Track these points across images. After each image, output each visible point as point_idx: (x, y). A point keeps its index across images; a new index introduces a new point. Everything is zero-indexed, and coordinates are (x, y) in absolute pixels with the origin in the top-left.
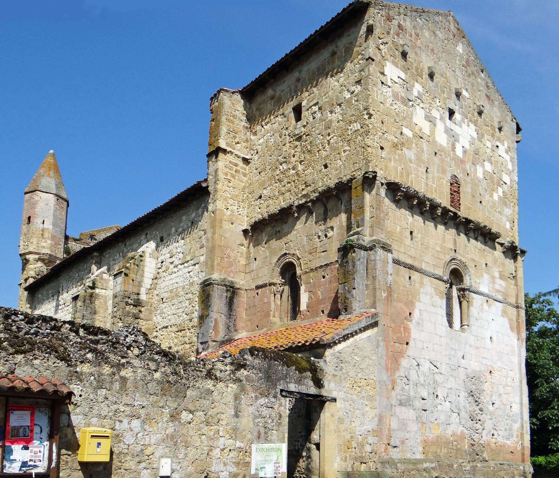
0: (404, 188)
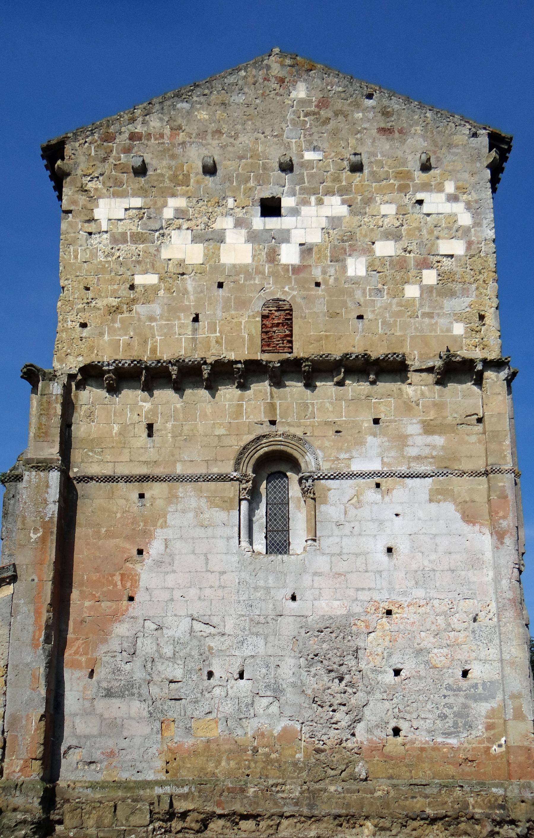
0: (108, 365)
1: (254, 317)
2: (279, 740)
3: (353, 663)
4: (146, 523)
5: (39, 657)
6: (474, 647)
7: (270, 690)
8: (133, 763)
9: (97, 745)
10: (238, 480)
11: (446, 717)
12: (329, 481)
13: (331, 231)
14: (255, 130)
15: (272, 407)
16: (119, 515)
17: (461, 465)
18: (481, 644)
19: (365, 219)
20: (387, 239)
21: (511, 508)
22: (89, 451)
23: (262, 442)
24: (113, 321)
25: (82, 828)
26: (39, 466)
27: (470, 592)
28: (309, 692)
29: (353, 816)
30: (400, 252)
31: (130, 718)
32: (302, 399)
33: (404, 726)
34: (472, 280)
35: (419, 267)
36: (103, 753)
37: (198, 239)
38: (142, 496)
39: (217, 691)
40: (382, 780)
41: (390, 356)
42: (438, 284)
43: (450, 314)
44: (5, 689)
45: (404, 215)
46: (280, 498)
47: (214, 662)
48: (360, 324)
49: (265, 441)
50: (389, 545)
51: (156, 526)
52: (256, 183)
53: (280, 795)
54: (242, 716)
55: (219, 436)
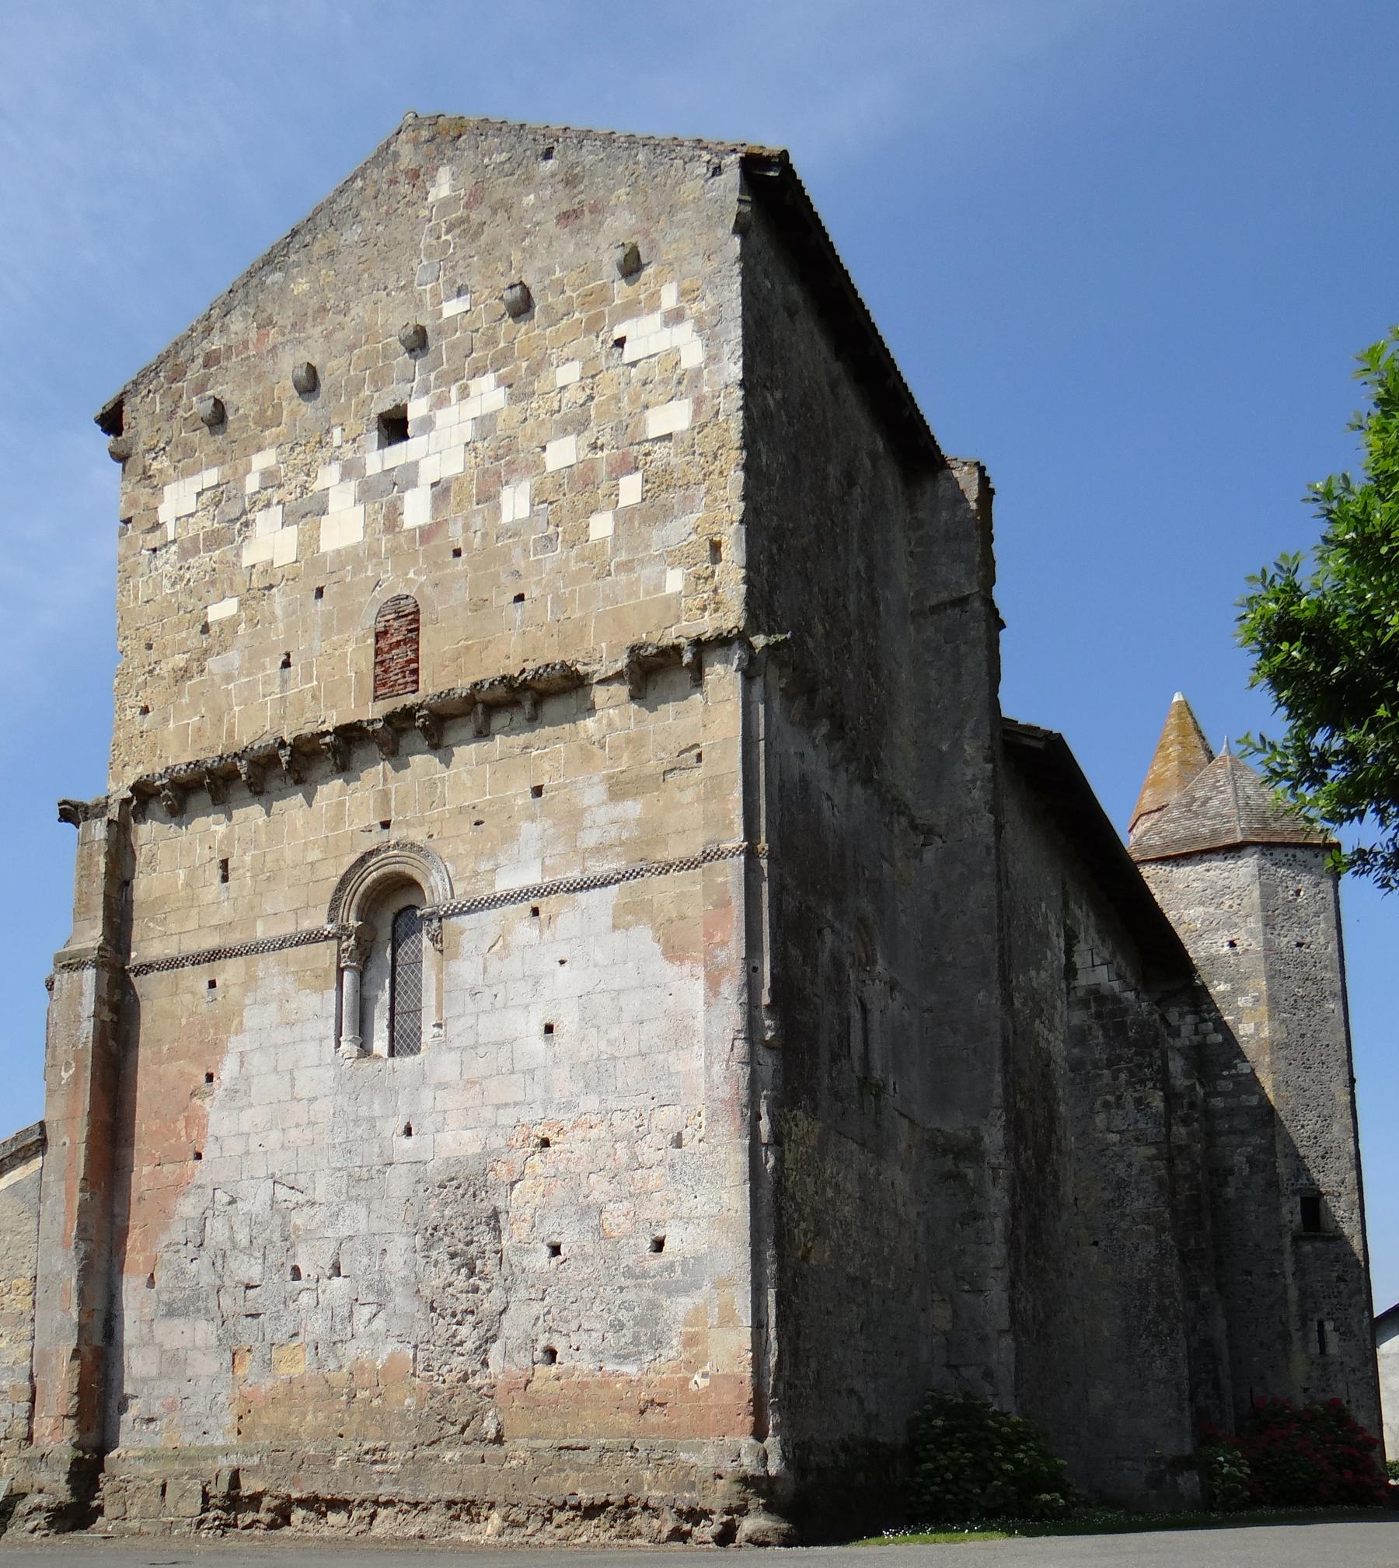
1: (364, 638)
2: (384, 1377)
3: (487, 1238)
4: (216, 1027)
5: (71, 1261)
6: (672, 1196)
7: (373, 1293)
8: (199, 1419)
9: (156, 1393)
10: (334, 936)
11: (622, 1326)
12: (463, 917)
13: (479, 445)
14: (375, 287)
15: (385, 795)
16: (184, 1021)
17: (666, 849)
18: (684, 1189)
19: (533, 405)
20: (565, 432)
21: (735, 924)
22: (149, 920)
23: (370, 864)
24: (180, 694)
25: (124, 1519)
26: (70, 965)
27: (671, 1092)
28: (426, 1292)
29: (473, 1502)
30: (586, 454)
31: (195, 1348)
32: (427, 775)
33: (560, 1345)
34: (701, 476)
35: (614, 475)
36: (163, 1405)
37: (291, 519)
38: (212, 984)
39: (306, 1299)
40: (521, 1441)
41: (541, 671)
42: (643, 500)
43: (660, 555)
44: (33, 1312)
45: (593, 377)
46: (413, 952)
47: (300, 1251)
48: (518, 612)
49: (374, 860)
50: (547, 1021)
51: (229, 1031)
52: (372, 388)
53: (379, 1467)
54: (336, 1338)
55: (312, 864)
